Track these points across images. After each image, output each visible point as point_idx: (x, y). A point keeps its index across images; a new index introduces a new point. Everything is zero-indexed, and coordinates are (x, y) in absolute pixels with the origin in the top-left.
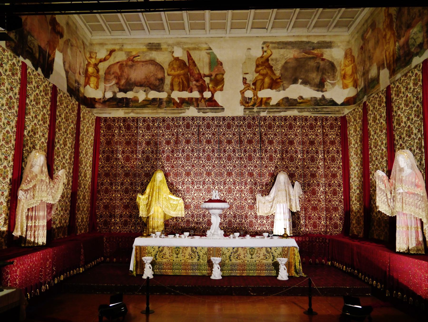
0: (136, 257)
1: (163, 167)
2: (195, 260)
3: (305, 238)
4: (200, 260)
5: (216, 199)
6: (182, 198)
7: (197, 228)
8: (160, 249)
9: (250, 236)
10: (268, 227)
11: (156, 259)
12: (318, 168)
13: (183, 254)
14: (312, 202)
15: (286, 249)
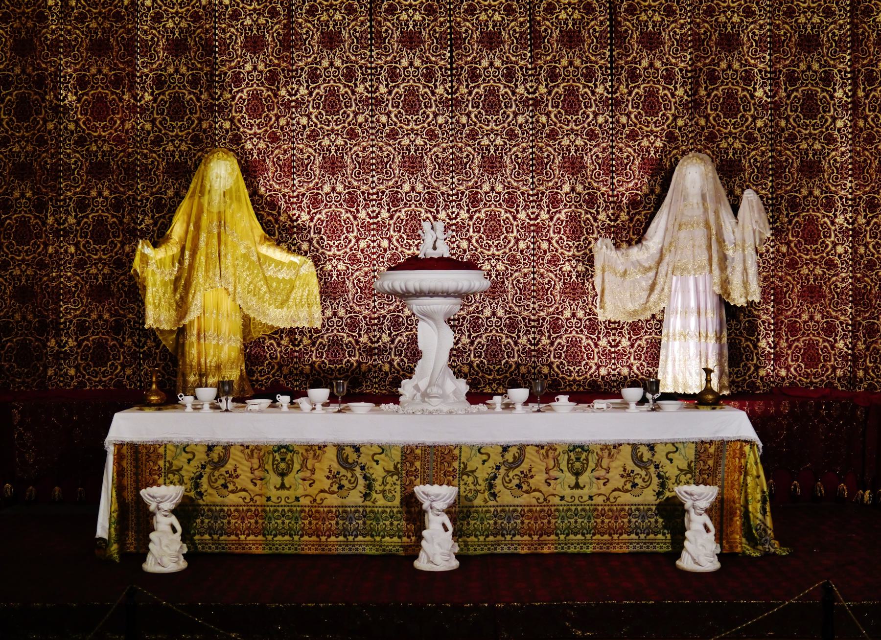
0: (120, 488)
1: (237, 140)
2: (355, 498)
3: (777, 406)
4: (374, 495)
5: (436, 255)
6: (313, 257)
7: (370, 370)
8: (215, 456)
9: (570, 400)
10: (636, 363)
11: (201, 494)
12: (830, 140)
13: (308, 474)
14: (805, 271)
15: (712, 450)
